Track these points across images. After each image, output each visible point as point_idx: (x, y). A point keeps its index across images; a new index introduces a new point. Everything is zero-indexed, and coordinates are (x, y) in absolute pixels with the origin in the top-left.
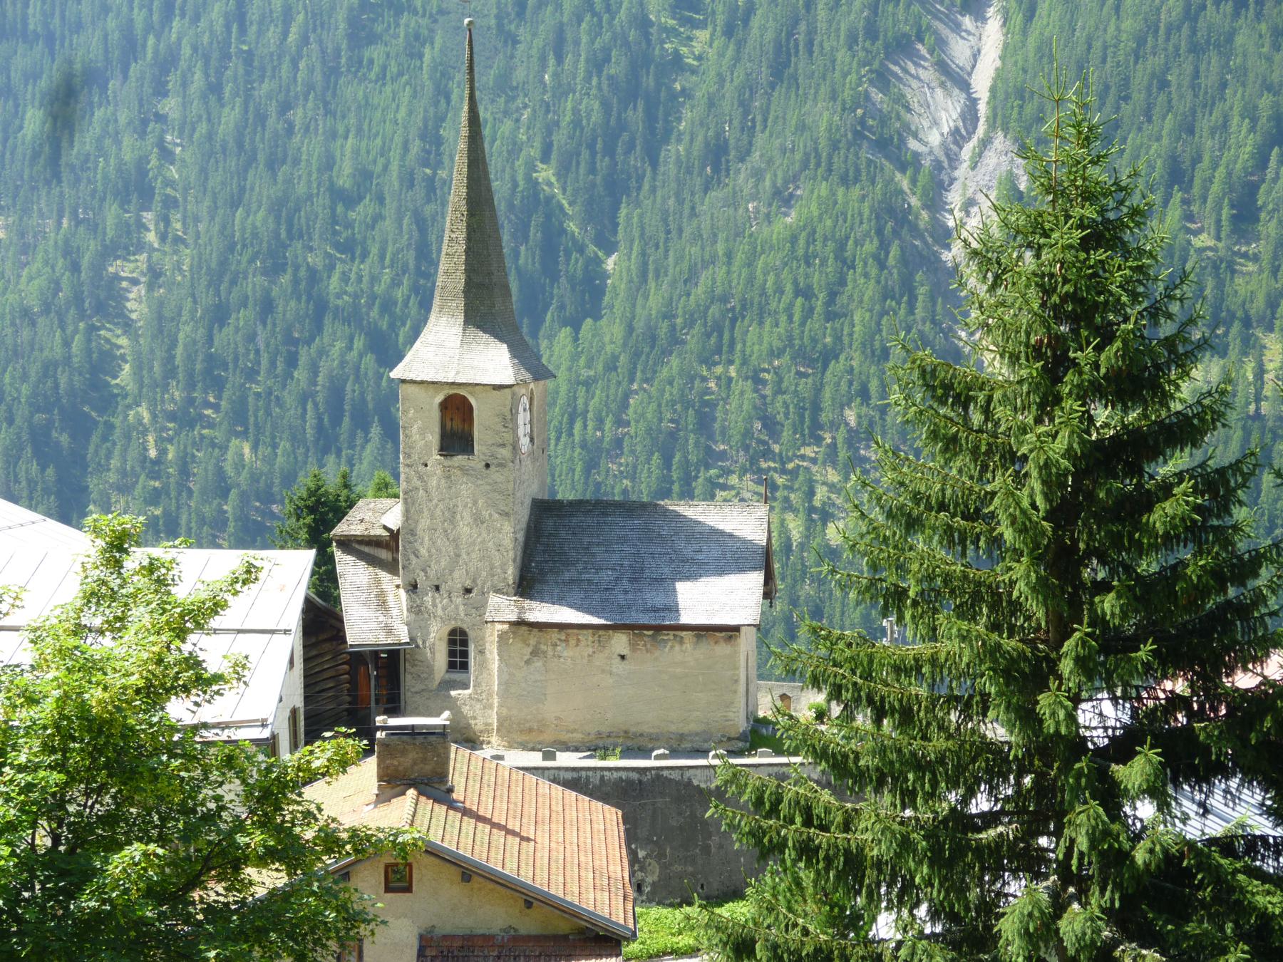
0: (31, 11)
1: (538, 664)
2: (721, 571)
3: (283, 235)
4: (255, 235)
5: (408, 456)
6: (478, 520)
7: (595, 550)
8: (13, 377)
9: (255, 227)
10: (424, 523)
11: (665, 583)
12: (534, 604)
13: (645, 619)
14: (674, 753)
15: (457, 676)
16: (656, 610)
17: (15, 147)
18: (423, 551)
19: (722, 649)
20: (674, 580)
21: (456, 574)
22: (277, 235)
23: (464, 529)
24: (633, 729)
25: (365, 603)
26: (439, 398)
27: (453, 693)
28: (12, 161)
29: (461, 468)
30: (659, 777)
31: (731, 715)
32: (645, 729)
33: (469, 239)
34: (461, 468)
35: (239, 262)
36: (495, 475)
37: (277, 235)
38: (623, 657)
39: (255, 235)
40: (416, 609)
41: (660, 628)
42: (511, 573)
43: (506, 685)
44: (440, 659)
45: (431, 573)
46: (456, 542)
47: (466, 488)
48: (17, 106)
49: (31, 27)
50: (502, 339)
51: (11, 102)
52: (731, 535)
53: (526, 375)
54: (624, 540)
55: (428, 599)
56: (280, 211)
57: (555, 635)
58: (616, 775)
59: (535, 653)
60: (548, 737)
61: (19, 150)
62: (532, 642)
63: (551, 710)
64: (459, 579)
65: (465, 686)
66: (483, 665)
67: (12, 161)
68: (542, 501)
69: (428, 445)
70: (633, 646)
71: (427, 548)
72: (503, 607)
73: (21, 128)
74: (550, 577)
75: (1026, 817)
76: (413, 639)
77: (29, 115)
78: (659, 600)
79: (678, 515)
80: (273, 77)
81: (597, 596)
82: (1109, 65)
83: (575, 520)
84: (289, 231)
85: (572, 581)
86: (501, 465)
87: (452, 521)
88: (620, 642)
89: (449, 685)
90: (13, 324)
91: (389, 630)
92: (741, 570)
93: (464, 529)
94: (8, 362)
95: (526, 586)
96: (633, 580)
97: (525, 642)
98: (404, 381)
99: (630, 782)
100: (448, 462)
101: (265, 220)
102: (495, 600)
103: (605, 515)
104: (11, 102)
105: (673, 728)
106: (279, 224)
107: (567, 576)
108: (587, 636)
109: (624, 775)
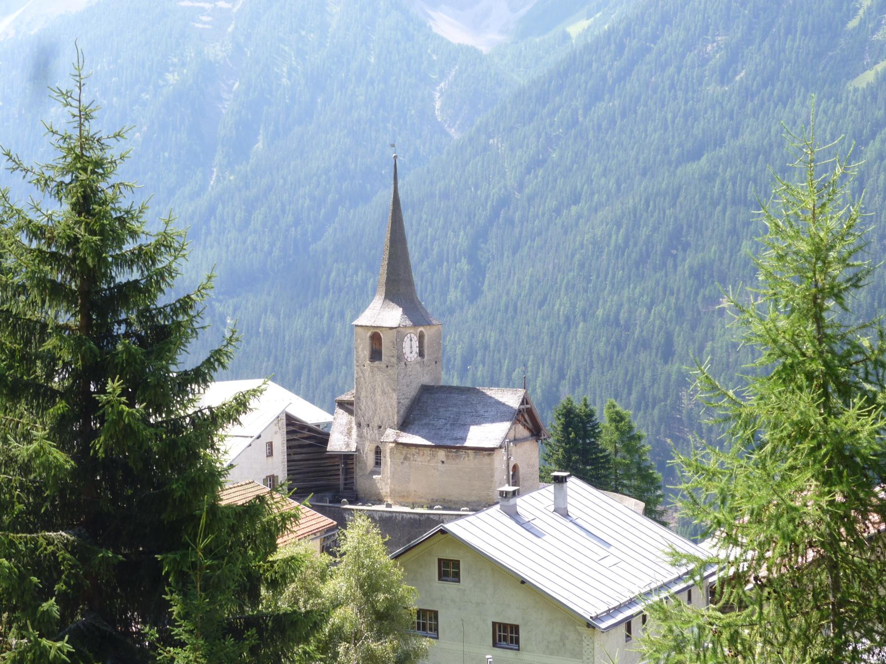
0: (749, 190)
1: (407, 463)
2: (493, 421)
3: (876, 304)
4: (860, 306)
5: (357, 361)
6: (384, 393)
7: (441, 410)
8: (725, 379)
9: (859, 301)
10: (363, 394)
11: (465, 427)
12: (404, 434)
13: (449, 443)
14: (444, 508)
15: (377, 469)
16: (456, 439)
17: (736, 260)
18: (363, 407)
19: (486, 460)
20: (470, 425)
21: (375, 419)
22: (872, 305)
23: (378, 397)
24: (447, 498)
25: (341, 433)
26: (369, 334)
27: (374, 477)
28: (734, 267)
29: (377, 367)
30: (428, 518)
31: (490, 493)
32: (453, 498)
33: (389, 258)
34: (377, 367)
35: (850, 320)
36: (390, 371)
37: (872, 305)
38: (443, 462)
39: (860, 306)
40: (360, 436)
41: (457, 449)
42: (396, 419)
43: (393, 474)
44: (370, 459)
45: (366, 418)
46: (375, 403)
47: (379, 377)
48: (738, 239)
49: (749, 198)
50: (399, 305)
51: (735, 237)
52: (504, 404)
53: (409, 323)
54: (455, 405)
55: (365, 431)
56: (875, 292)
57: (413, 450)
58: (409, 516)
59: (405, 458)
60: (411, 500)
61: (738, 262)
62: (404, 452)
63: (412, 487)
64: (376, 422)
65: (379, 473)
66: (385, 464)
67: (734, 267)
68: (426, 386)
69: (365, 356)
70: (447, 456)
71: (364, 404)
72: (391, 435)
73: (740, 250)
74: (416, 422)
75: (198, 490)
76: (357, 450)
77: (744, 243)
78: (459, 434)
79: (483, 394)
80: (877, 221)
81: (433, 432)
82: (692, 168)
83: (436, 395)
84: (879, 303)
85: (426, 424)
86: (392, 366)
87: (374, 393)
88: (441, 454)
89: (374, 473)
90: (727, 351)
91: (348, 445)
92: (502, 421)
93: (378, 397)
94: (723, 370)
95: (404, 426)
96: (452, 425)
97: (401, 453)
98: (357, 326)
99: (415, 520)
100: (372, 365)
101: (865, 297)
102: (389, 431)
103: (451, 393)
104: (735, 237)
105: (465, 499)
106: (874, 300)
107: (424, 422)
108: (427, 451)
109: (412, 516)
